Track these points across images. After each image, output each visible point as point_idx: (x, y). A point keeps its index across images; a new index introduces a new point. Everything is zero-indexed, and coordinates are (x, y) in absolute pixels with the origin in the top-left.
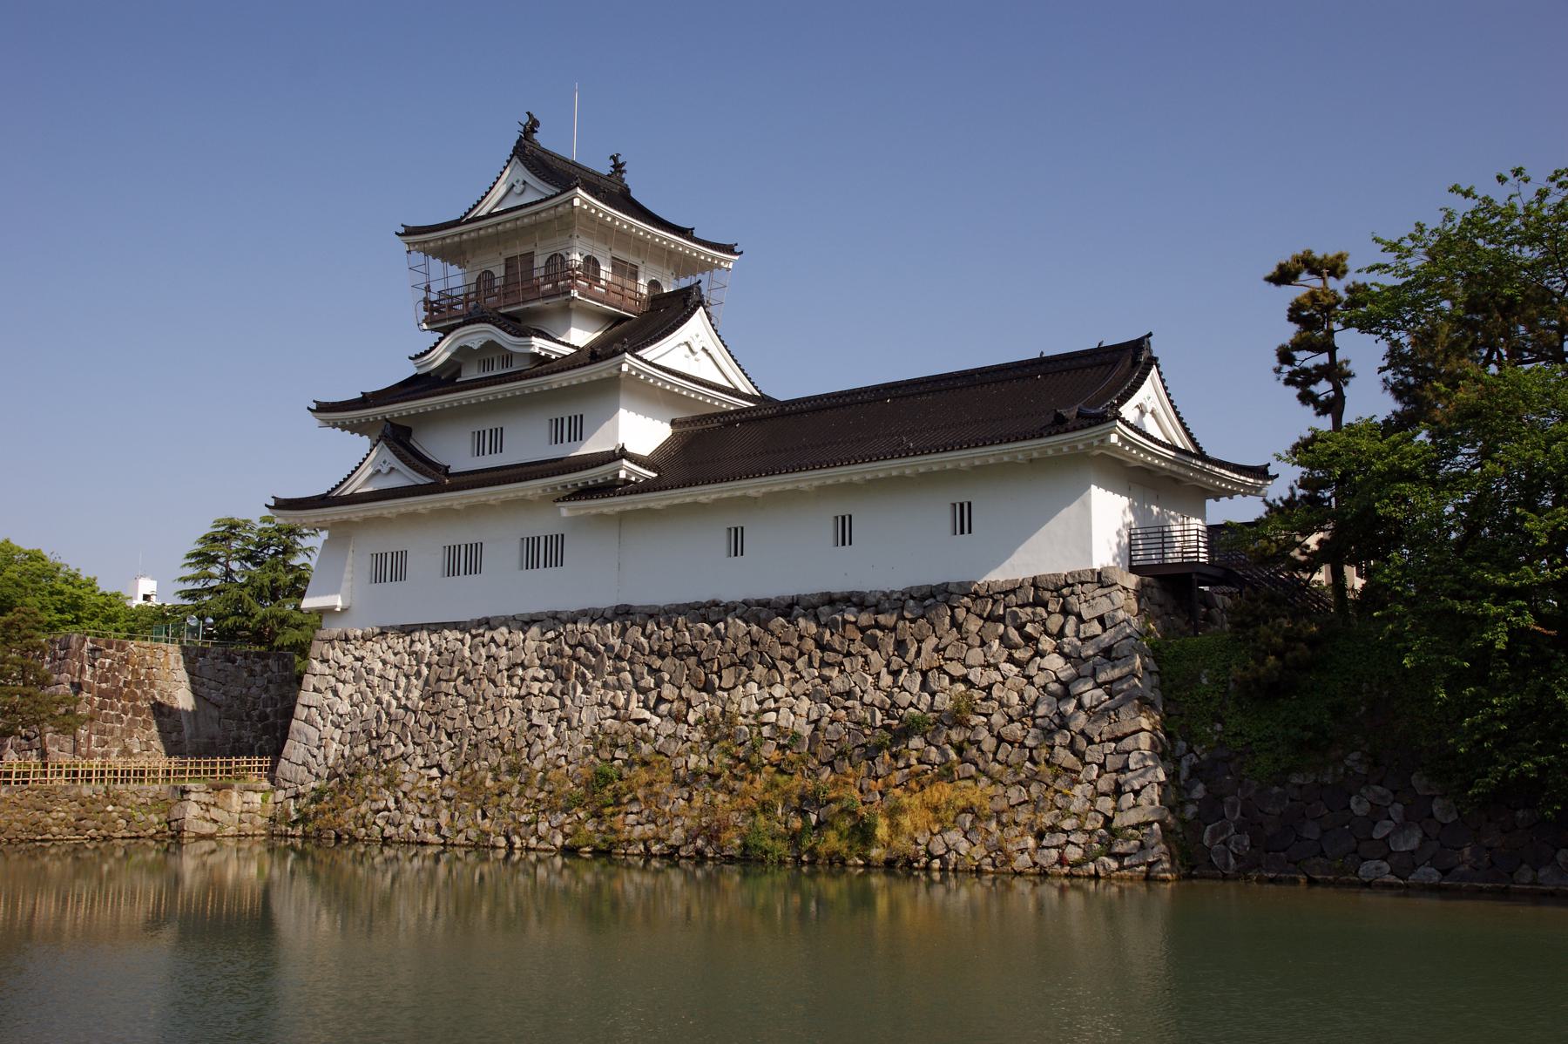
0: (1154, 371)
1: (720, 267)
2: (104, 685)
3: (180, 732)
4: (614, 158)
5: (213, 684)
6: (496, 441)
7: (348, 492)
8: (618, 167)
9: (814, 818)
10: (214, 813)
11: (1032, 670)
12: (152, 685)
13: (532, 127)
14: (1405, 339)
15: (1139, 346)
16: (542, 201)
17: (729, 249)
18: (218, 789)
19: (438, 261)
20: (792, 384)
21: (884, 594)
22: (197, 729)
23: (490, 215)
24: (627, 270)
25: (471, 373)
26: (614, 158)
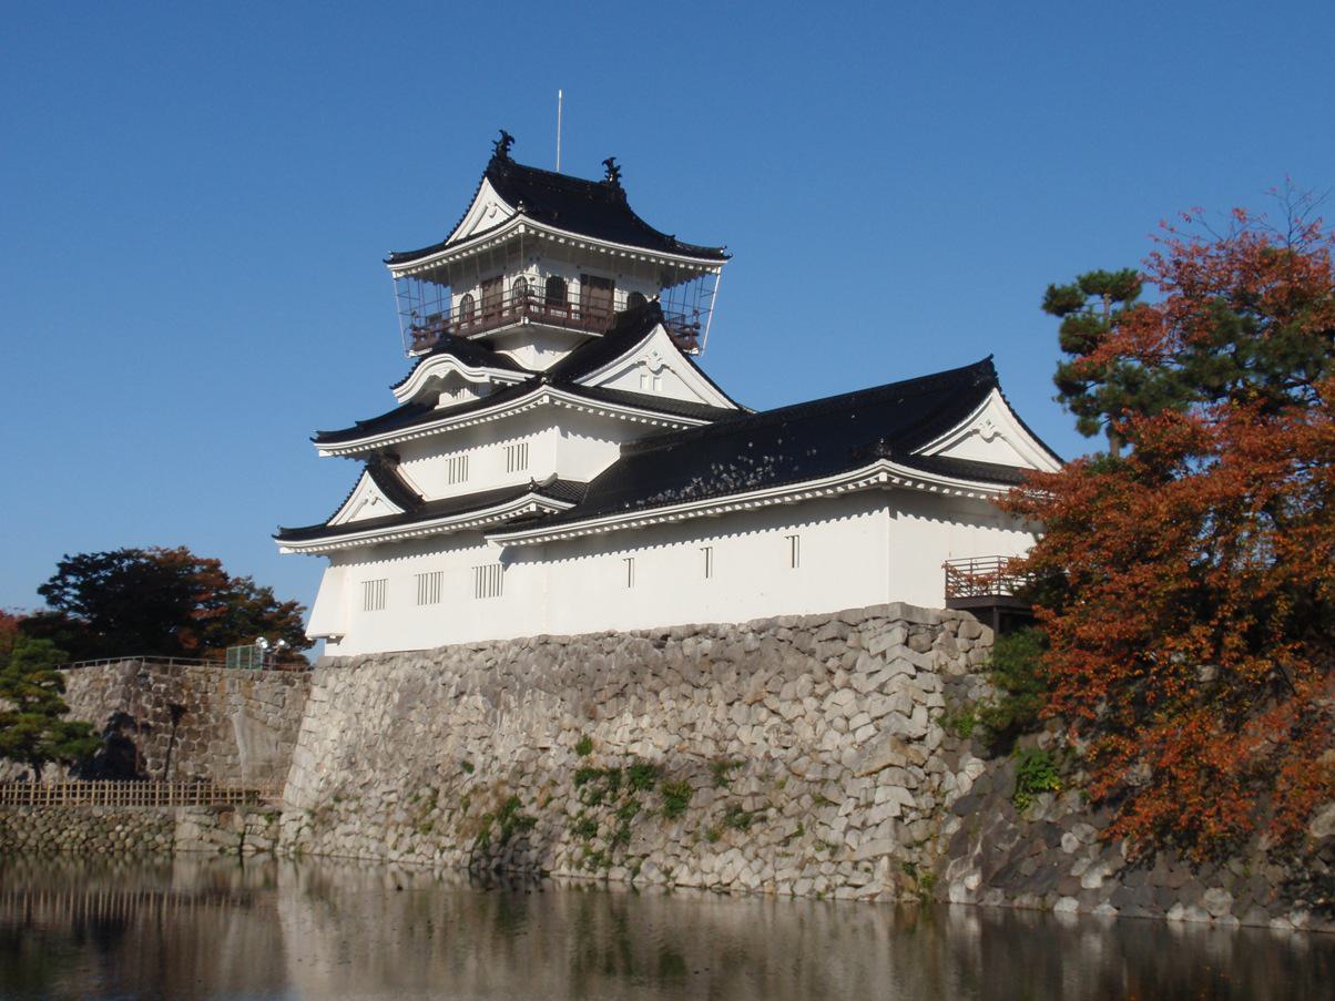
0: (399, 511)
1: (710, 273)
2: (159, 710)
3: (236, 755)
4: (609, 163)
5: (270, 707)
6: (521, 460)
7: (342, 522)
8: (614, 171)
9: (1298, 860)
10: (217, 834)
11: (827, 705)
12: (207, 709)
13: (507, 139)
14: (1200, 354)
15: (987, 365)
16: (509, 220)
17: (713, 254)
18: (220, 810)
19: (430, 284)
20: (763, 399)
21: (733, 627)
22: (253, 752)
23: (469, 238)
24: (598, 283)
25: (446, 401)
26: (609, 163)
